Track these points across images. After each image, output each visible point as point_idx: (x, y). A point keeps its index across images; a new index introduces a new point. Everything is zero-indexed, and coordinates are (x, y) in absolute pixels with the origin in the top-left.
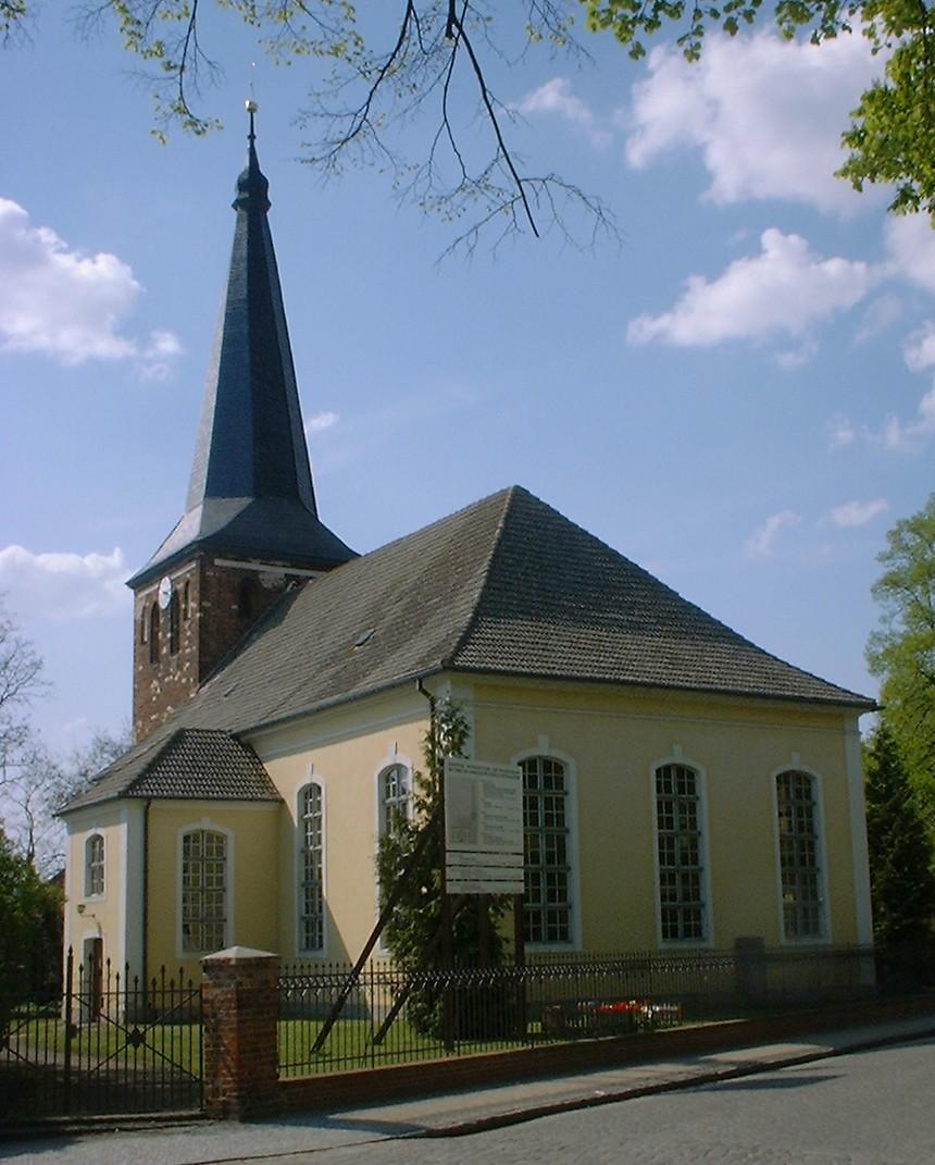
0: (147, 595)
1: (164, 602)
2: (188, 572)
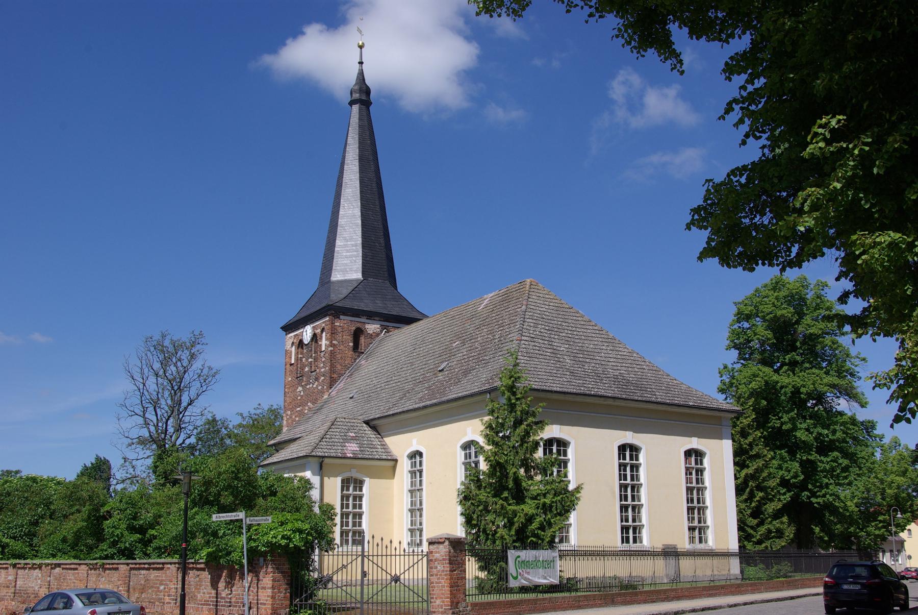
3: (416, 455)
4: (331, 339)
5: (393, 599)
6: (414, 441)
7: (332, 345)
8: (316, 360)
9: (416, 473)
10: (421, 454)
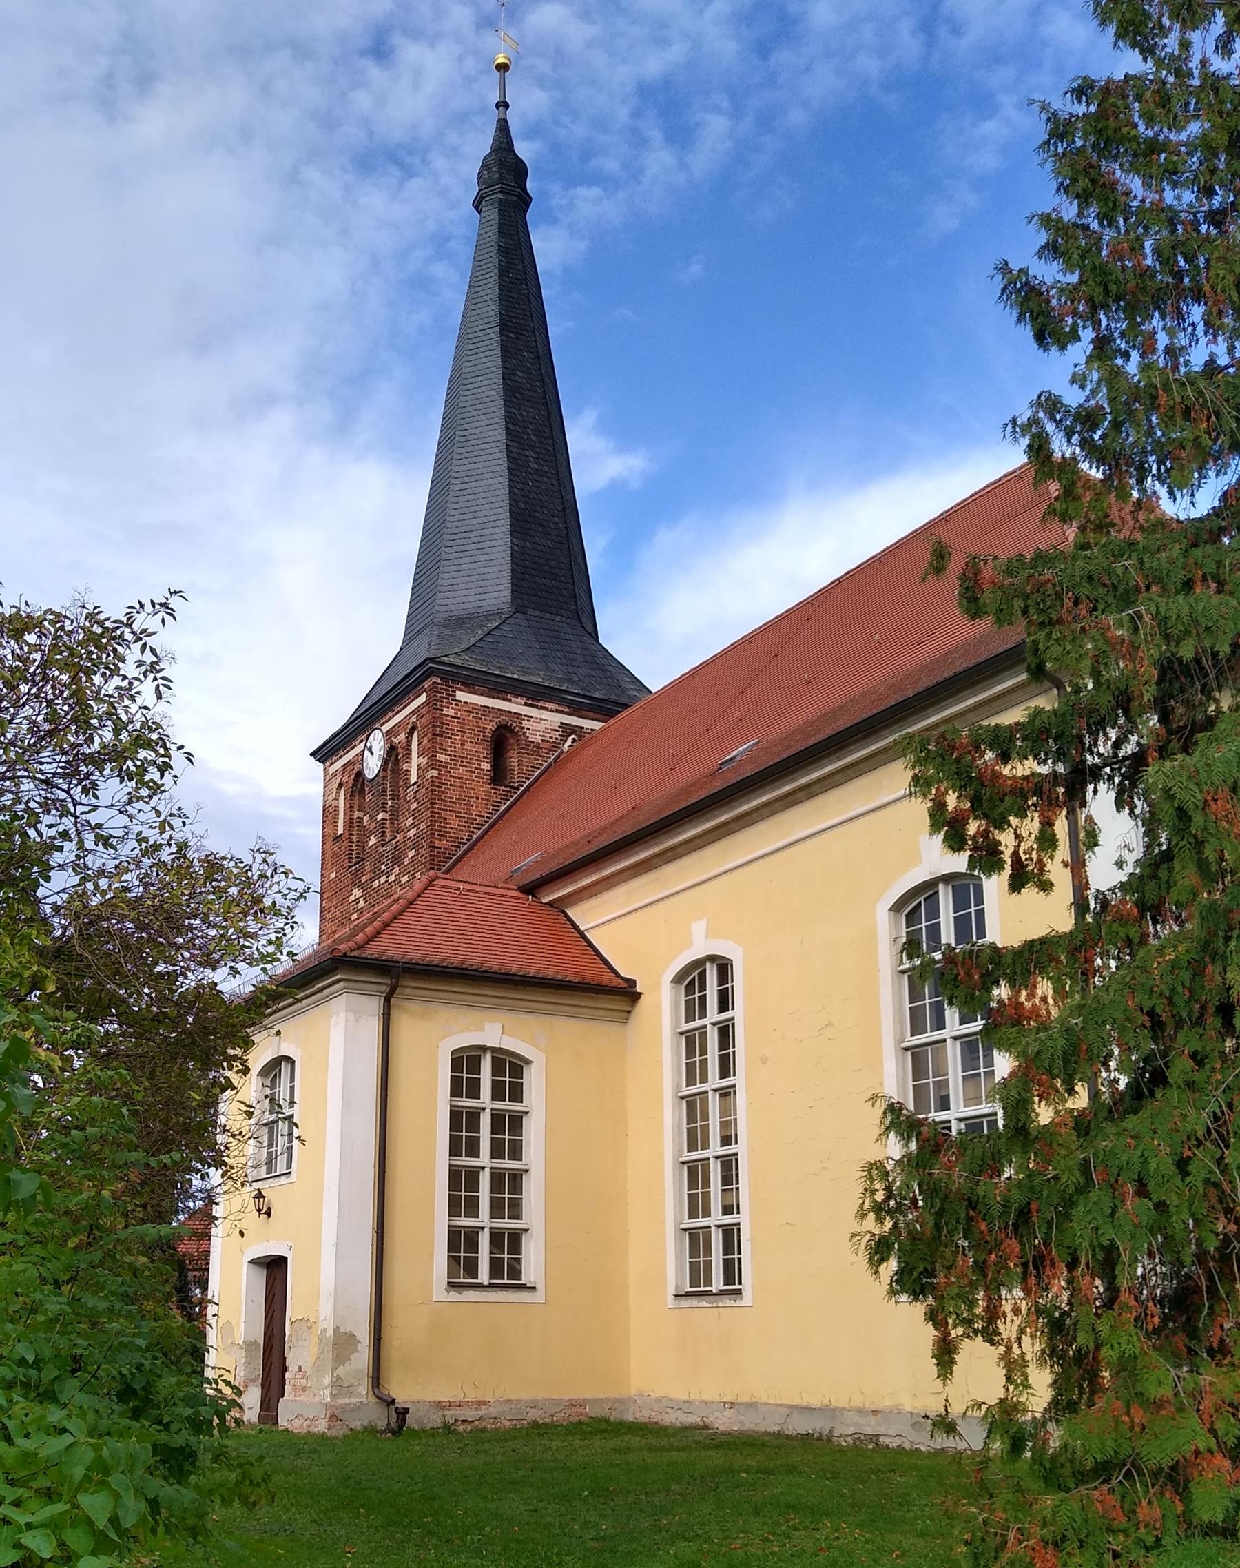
0: (345, 766)
1: (372, 766)
2: (413, 713)
3: (706, 981)
4: (429, 753)
5: (445, 556)
6: (699, 929)
7: (433, 764)
8: (395, 814)
9: (710, 1049)
10: (724, 968)
